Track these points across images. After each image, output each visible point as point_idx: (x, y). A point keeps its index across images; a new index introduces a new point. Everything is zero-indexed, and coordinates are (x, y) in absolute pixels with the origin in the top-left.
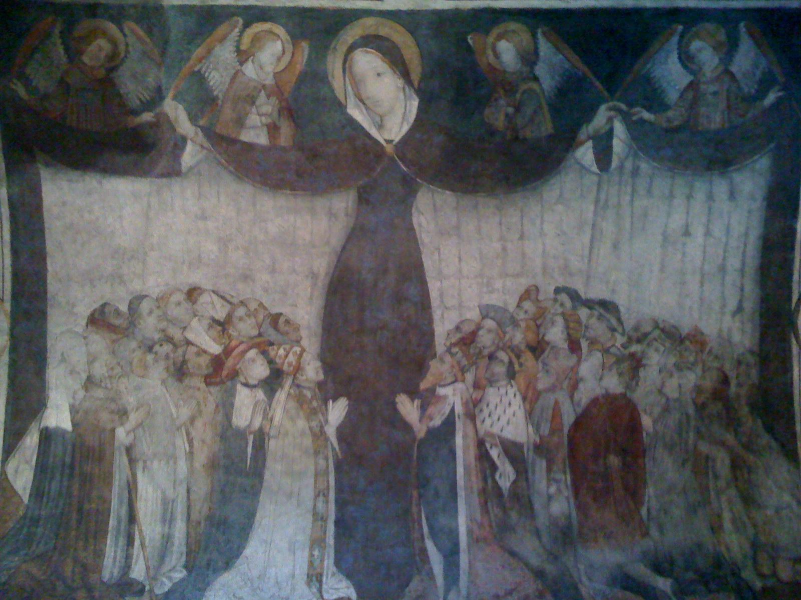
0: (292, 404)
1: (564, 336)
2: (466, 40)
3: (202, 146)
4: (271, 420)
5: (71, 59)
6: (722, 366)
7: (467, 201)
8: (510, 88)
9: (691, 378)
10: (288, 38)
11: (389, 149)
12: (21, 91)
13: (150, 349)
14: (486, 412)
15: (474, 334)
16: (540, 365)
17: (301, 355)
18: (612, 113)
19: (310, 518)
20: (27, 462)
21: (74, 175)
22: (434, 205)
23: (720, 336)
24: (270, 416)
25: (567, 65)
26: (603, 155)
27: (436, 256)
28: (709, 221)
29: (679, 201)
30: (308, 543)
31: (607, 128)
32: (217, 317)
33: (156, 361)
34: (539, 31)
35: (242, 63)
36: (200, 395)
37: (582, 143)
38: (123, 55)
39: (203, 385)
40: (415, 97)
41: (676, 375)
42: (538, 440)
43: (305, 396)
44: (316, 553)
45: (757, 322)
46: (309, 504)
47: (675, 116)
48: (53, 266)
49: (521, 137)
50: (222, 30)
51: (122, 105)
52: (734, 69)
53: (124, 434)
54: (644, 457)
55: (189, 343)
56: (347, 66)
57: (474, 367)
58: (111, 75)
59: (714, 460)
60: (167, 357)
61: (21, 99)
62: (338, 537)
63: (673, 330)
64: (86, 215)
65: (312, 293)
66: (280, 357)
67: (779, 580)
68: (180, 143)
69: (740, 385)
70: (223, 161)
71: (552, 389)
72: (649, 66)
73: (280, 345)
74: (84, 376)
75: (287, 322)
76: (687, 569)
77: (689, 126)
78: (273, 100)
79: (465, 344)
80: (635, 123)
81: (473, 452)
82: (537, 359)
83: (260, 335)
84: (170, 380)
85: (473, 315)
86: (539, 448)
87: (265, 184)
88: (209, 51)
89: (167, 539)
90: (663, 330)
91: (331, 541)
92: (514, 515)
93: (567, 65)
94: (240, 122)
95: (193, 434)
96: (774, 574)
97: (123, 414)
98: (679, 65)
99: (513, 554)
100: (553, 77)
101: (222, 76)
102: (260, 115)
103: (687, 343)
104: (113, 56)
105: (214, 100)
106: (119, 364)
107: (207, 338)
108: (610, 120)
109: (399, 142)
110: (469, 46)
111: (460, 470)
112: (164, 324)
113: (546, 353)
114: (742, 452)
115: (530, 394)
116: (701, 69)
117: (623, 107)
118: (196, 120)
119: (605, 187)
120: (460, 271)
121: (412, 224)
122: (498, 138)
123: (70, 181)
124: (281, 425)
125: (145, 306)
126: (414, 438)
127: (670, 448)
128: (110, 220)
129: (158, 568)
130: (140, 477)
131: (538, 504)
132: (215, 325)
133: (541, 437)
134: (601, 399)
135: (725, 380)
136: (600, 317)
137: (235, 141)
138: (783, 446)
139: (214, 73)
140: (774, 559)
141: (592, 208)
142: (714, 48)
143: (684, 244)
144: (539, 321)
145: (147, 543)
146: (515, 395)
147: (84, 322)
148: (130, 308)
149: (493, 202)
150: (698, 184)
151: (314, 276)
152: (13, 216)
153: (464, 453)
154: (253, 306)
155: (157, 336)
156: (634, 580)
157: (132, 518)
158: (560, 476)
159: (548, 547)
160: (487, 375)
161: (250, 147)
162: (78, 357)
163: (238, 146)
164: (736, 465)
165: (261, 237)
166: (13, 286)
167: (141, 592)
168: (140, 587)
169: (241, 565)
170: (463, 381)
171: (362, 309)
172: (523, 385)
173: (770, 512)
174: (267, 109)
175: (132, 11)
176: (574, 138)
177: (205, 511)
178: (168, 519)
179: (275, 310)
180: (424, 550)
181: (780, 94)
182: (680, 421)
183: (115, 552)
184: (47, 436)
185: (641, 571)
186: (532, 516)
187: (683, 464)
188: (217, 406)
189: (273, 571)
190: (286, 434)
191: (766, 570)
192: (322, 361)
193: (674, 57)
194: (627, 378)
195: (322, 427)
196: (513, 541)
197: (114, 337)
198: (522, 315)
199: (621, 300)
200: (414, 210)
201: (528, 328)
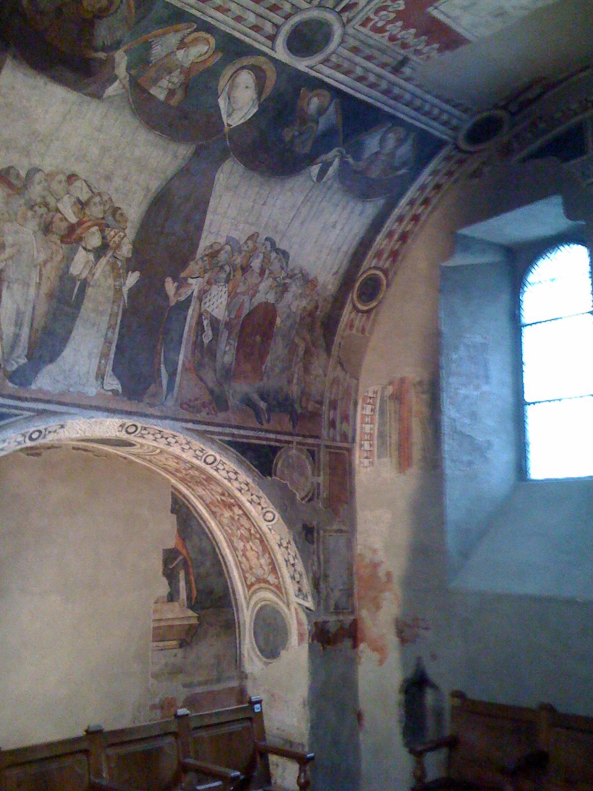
0: (108, 268)
8: (304, 121)
9: (304, 303)
11: (227, 129)
14: (207, 300)
15: (218, 252)
17: (122, 239)
18: (338, 153)
19: (103, 339)
21: (31, 72)
23: (323, 285)
27: (218, 200)
32: (81, 199)
33: (34, 217)
34: (335, 101)
36: (54, 247)
38: (112, 12)
40: (257, 106)
42: (228, 320)
44: (103, 362)
46: (104, 332)
47: (362, 165)
55: (58, 210)
56: (235, 75)
57: (211, 271)
64: (24, 102)
68: (113, 79)
69: (321, 311)
70: (131, 100)
71: (243, 294)
75: (122, 215)
78: (182, 77)
83: (103, 218)
84: (40, 234)
85: (222, 241)
86: (228, 325)
87: (147, 123)
88: (164, 34)
89: (17, 336)
91: (112, 356)
92: (206, 359)
94: (155, 81)
95: (44, 272)
96: (306, 408)
99: (201, 379)
101: (162, 50)
102: (169, 81)
105: (149, 62)
106: (8, 212)
107: (70, 211)
108: (336, 156)
111: (187, 328)
112: (46, 193)
113: (249, 272)
115: (232, 294)
118: (130, 69)
119: (314, 190)
120: (225, 213)
123: (25, 74)
124: (98, 279)
125: (38, 177)
128: (40, 111)
132: (78, 203)
133: (230, 318)
135: (317, 307)
136: (280, 260)
137: (145, 91)
140: (308, 400)
141: (303, 198)
144: (252, 254)
146: (225, 293)
148: (27, 175)
154: (106, 198)
155: (39, 200)
158: (232, 342)
160: (216, 278)
161: (152, 97)
164: (307, 351)
165: (128, 155)
169: (60, 360)
170: (203, 278)
172: (230, 288)
174: (175, 80)
176: (315, 159)
177: (42, 323)
178: (18, 324)
180: (159, 370)
185: (256, 397)
187: (286, 347)
189: (77, 368)
191: (304, 405)
192: (134, 246)
194: (278, 295)
197: (10, 191)
198: (245, 248)
199: (292, 254)
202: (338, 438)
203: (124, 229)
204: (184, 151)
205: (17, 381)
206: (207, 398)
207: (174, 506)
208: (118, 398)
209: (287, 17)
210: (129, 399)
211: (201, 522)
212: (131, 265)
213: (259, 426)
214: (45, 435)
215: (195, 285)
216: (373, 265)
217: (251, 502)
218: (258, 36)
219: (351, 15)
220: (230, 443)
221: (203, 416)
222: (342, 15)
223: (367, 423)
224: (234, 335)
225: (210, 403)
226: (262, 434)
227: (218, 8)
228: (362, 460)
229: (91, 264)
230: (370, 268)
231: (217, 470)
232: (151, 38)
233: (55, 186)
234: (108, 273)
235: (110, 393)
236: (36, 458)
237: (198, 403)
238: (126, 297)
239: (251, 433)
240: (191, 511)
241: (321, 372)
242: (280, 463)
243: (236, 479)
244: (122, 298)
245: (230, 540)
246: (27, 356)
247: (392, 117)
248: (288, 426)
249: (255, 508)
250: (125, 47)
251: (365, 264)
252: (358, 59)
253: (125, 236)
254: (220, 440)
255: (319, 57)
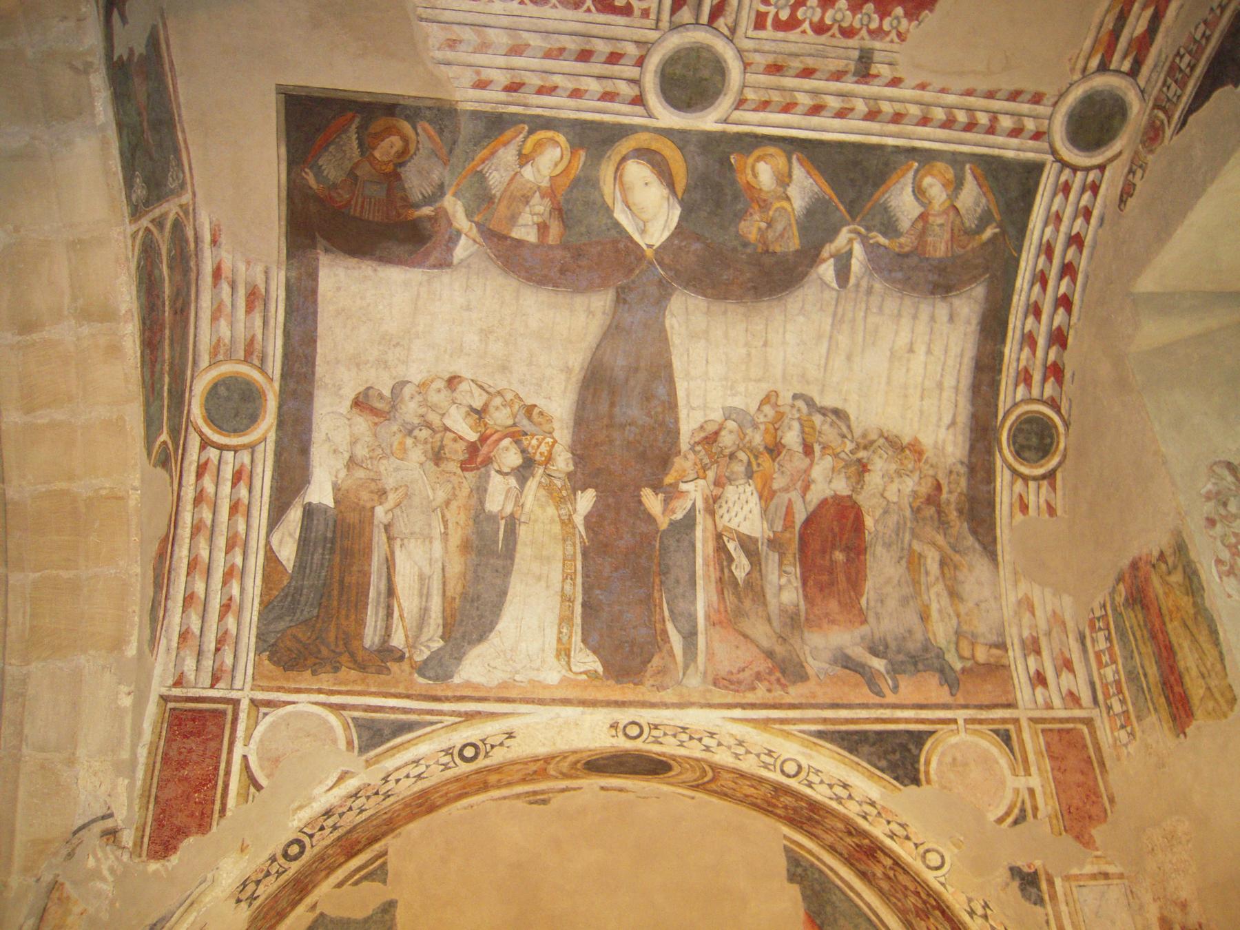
0: (542, 492)
1: (799, 440)
2: (728, 159)
3: (474, 241)
4: (523, 506)
5: (362, 153)
6: (936, 473)
7: (718, 307)
9: (909, 484)
10: (568, 146)
11: (649, 253)
12: (311, 179)
13: (410, 433)
14: (725, 507)
16: (777, 466)
17: (553, 446)
18: (853, 235)
19: (558, 598)
20: (291, 535)
22: (687, 309)
23: (935, 446)
24: (522, 501)
25: (816, 189)
26: (843, 273)
28: (930, 340)
29: (906, 322)
30: (557, 621)
31: (847, 248)
34: (794, 157)
35: (521, 166)
36: (455, 480)
37: (824, 261)
39: (459, 471)
41: (897, 480)
42: (772, 535)
43: (555, 485)
44: (565, 630)
45: (968, 435)
46: (558, 587)
47: (906, 242)
48: (323, 349)
49: (770, 250)
50: (508, 134)
51: (405, 199)
52: (958, 205)
53: (383, 514)
54: (865, 554)
55: (447, 429)
58: (399, 170)
59: (925, 558)
60: (426, 442)
61: (311, 188)
62: (585, 616)
63: (896, 439)
65: (566, 387)
66: (533, 447)
67: (977, 663)
69: (950, 492)
71: (786, 490)
72: (886, 196)
73: (533, 435)
74: (347, 456)
75: (541, 413)
76: (899, 652)
77: (918, 251)
78: (547, 200)
79: (708, 443)
80: (872, 245)
81: (711, 545)
82: (774, 461)
83: (514, 425)
84: (430, 465)
85: (717, 416)
86: (773, 543)
87: (529, 279)
88: (493, 153)
89: (424, 612)
90: (886, 439)
91: (578, 620)
92: (748, 603)
93: (816, 189)
94: (513, 219)
95: (448, 515)
96: (973, 656)
97: (382, 494)
98: (912, 198)
99: (745, 636)
100: (803, 199)
103: (907, 452)
104: (404, 152)
107: (464, 425)
108: (851, 241)
109: (659, 247)
110: (731, 164)
113: (782, 455)
114: (950, 552)
115: (766, 493)
116: (930, 202)
117: (863, 230)
120: (706, 373)
121: (664, 326)
122: (749, 251)
125: (408, 391)
126: (657, 531)
127: (888, 546)
128: (381, 307)
129: (417, 637)
130: (398, 553)
131: (769, 597)
134: (830, 501)
136: (832, 424)
137: (505, 237)
138: (985, 548)
139: (495, 173)
141: (829, 321)
142: (943, 185)
143: (909, 360)
145: (405, 615)
147: (348, 403)
149: (741, 309)
150: (922, 306)
151: (568, 370)
152: (288, 298)
153: (703, 545)
154: (509, 396)
155: (416, 421)
156: (853, 660)
157: (391, 592)
158: (790, 569)
159: (778, 630)
161: (520, 243)
162: (341, 438)
163: (509, 242)
166: (283, 365)
167: (402, 658)
168: (399, 654)
169: (494, 638)
170: (705, 478)
171: (612, 405)
172: (760, 486)
173: (971, 604)
175: (428, 113)
176: (818, 255)
177: (459, 588)
178: (425, 595)
179: (529, 402)
181: (997, 230)
182: (898, 523)
183: (376, 622)
184: (310, 512)
185: (859, 653)
186: (765, 604)
188: (471, 491)
190: (536, 521)
191: (967, 653)
192: (572, 453)
193: (909, 190)
194: (853, 480)
195: (570, 515)
196: (746, 626)
197: (376, 420)
200: (667, 313)
201: (766, 431)
202: (1057, 702)
203: (550, 433)
204: (602, 301)
205: (432, 674)
206: (763, 665)
207: (792, 869)
208: (597, 683)
209: (640, 62)
210: (618, 682)
211: (851, 894)
212: (577, 482)
213: (877, 700)
214: (487, 753)
215: (695, 492)
216: (1019, 397)
217: (892, 836)
218: (616, 106)
219: (730, 21)
220: (820, 735)
221: (760, 694)
222: (715, 25)
223: (1107, 665)
224: (790, 557)
225: (771, 673)
226: (887, 713)
227: (540, 91)
228: (1116, 734)
229: (514, 492)
230: (1016, 405)
231: (810, 785)
232: (478, 165)
233: (434, 397)
234: (543, 499)
235: (584, 677)
236: (542, 806)
237: (747, 675)
238: (582, 529)
239: (863, 714)
240: (826, 876)
241: (986, 593)
242: (933, 759)
243: (850, 797)
244: (577, 532)
245: (907, 920)
246: (442, 637)
247: (912, 151)
248: (944, 695)
249: (901, 845)
250: (452, 189)
251: (1004, 402)
252: (789, 82)
253: (555, 442)
254: (801, 731)
255: (725, 104)
